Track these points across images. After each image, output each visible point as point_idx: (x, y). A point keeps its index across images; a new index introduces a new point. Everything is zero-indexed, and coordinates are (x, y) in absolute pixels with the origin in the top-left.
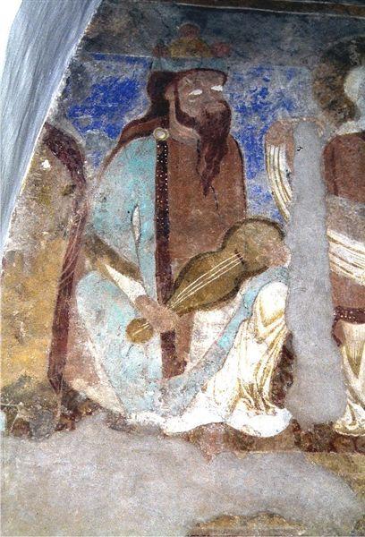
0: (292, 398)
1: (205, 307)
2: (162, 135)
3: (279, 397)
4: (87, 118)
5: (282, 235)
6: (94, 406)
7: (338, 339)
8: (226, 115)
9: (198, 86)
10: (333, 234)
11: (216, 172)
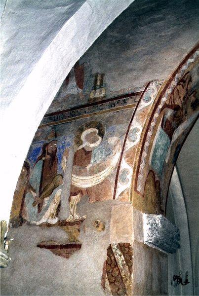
0: (59, 215)
1: (46, 197)
2: (44, 159)
3: (57, 215)
4: (31, 158)
5: (63, 178)
6: (25, 220)
7: (70, 200)
8: (56, 151)
9: (52, 145)
10: (73, 175)
11: (53, 165)
